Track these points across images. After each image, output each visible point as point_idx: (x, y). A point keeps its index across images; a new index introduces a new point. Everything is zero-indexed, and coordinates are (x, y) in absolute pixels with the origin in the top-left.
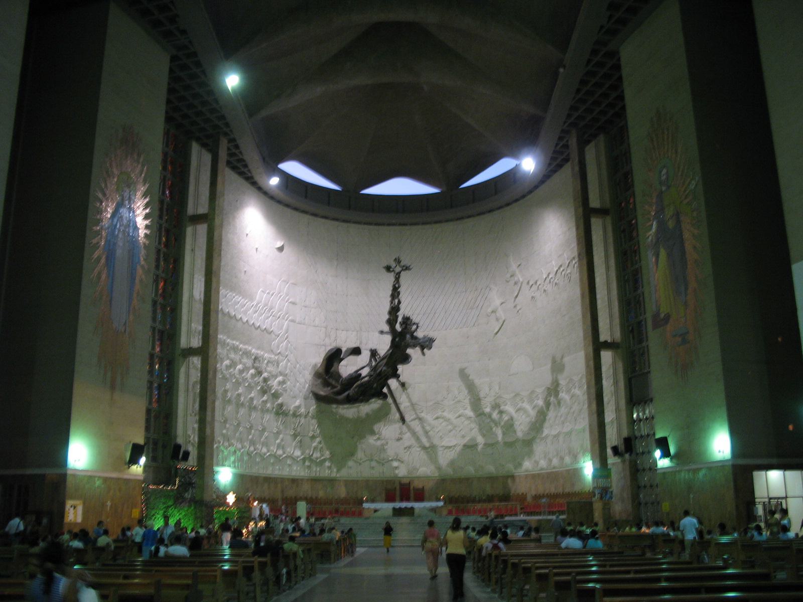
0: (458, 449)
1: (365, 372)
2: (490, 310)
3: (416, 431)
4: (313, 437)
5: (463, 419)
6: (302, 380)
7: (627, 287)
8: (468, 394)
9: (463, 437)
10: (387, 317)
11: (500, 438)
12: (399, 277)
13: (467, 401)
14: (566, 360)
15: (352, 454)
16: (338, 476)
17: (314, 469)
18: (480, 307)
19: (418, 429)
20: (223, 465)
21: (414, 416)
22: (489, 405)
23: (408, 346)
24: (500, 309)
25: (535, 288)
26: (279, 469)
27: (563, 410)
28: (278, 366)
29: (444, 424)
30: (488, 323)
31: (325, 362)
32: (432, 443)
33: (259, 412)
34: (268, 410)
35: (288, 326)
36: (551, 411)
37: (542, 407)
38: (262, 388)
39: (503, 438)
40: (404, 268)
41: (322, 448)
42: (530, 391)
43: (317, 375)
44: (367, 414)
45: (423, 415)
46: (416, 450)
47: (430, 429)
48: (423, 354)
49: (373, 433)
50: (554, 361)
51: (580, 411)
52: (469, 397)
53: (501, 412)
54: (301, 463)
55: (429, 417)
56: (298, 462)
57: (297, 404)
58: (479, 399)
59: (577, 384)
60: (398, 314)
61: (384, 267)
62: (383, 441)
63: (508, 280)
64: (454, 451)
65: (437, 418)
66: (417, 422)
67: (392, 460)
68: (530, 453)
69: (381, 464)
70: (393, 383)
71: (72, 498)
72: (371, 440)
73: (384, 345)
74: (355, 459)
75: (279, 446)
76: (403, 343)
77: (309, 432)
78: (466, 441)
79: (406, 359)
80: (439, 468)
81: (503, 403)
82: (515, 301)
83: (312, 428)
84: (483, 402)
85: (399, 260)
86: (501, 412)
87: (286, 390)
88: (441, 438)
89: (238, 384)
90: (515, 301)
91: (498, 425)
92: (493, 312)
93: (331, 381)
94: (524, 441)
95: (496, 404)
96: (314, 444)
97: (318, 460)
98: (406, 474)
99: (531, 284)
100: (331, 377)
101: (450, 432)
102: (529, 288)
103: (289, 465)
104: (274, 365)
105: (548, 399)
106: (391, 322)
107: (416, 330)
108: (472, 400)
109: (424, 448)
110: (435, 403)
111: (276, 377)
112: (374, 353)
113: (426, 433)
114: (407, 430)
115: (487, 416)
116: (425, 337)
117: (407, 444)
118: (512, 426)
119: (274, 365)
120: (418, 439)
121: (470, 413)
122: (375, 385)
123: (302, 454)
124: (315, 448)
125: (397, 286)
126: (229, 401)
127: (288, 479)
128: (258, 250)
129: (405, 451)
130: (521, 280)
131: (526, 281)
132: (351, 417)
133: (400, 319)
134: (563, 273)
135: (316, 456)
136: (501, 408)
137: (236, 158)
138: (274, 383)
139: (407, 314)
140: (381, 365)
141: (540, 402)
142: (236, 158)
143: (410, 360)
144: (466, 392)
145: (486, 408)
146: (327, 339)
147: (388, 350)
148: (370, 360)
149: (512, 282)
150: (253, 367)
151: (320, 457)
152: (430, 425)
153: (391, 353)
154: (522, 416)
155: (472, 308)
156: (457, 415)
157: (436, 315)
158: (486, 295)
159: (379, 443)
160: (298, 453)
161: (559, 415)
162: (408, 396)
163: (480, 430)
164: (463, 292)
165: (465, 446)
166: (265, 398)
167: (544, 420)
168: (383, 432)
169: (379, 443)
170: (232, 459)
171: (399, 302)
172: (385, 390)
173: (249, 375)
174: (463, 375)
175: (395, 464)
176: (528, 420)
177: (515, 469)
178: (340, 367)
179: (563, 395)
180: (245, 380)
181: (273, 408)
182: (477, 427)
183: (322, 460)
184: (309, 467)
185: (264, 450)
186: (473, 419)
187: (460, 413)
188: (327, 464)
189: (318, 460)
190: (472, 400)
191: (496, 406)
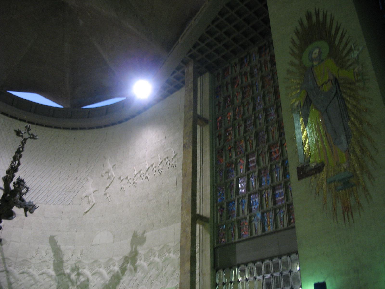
2: (84, 195)
5: (45, 276)
7: (218, 175)
8: (54, 256)
10: (5, 174)
12: (25, 142)
13: (52, 262)
14: (147, 234)
18: (76, 191)
22: (70, 267)
23: (15, 204)
24: (92, 195)
25: (125, 181)
27: (139, 274)
29: (28, 278)
30: (80, 204)
36: (127, 276)
37: (118, 272)
40: (31, 136)
42: (108, 259)
45: (11, 269)
50: (135, 235)
51: (174, 272)
52: (54, 259)
53: (79, 274)
55: (15, 271)
58: (62, 262)
59: (157, 254)
60: (15, 174)
61: (15, 131)
63: (103, 175)
65: (23, 273)
76: (13, 199)
81: (82, 266)
84: (65, 264)
85: (29, 128)
91: (75, 284)
92: (86, 196)
95: (76, 267)
99: (122, 178)
102: (120, 181)
105: (124, 266)
106: (7, 180)
108: (56, 262)
110: (24, 260)
115: (67, 276)
121: (52, 272)
125: (21, 149)
130: (114, 175)
131: (118, 177)
133: (15, 180)
134: (155, 169)
136: (80, 271)
139: (22, 177)
141: (116, 268)
143: (14, 217)
145: (67, 269)
149: (106, 177)
152: (15, 278)
154: (97, 279)
155: (70, 192)
157: (41, 192)
158: (82, 184)
161: (135, 278)
164: (65, 179)
167: (118, 283)
171: (19, 164)
174: (52, 240)
176: (102, 282)
179: (141, 262)
182: (56, 284)
186: (53, 277)
187: (44, 270)
190: (56, 262)
191: (76, 269)
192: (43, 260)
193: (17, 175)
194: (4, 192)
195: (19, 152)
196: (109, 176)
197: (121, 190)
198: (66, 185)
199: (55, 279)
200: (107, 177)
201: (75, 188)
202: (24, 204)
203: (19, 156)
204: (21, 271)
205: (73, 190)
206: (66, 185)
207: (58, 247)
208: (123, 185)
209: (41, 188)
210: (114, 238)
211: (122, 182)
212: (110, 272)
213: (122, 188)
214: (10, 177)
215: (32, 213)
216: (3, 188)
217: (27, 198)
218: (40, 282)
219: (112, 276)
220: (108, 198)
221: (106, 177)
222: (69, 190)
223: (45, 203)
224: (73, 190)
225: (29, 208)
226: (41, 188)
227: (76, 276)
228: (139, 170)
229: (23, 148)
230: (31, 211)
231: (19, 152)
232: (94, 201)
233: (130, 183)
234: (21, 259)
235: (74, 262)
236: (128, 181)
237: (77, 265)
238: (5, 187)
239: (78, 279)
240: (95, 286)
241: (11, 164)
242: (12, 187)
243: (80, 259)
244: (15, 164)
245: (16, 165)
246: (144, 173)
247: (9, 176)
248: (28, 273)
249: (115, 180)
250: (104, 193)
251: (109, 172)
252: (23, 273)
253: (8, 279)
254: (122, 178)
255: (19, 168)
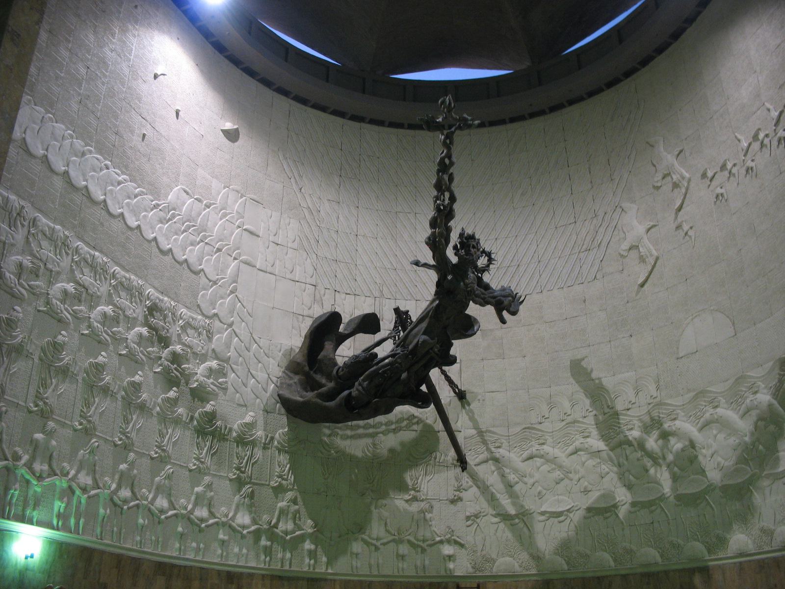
0: (577, 516)
2: (625, 246)
3: (489, 483)
4: (279, 490)
5: (583, 456)
6: (262, 376)
9: (586, 491)
10: (428, 232)
11: (667, 487)
12: (451, 143)
13: (590, 420)
15: (360, 528)
16: (330, 571)
17: (280, 555)
18: (604, 244)
19: (492, 479)
20: (22, 519)
21: (485, 455)
22: (637, 423)
24: (646, 240)
26: (198, 549)
28: (210, 339)
29: (546, 468)
31: (308, 341)
32: (522, 506)
33: (155, 420)
34: (177, 421)
35: (238, 270)
37: (770, 405)
38: (166, 371)
39: (674, 489)
41: (298, 511)
43: (293, 368)
44: (392, 451)
46: (490, 521)
47: (516, 479)
49: (402, 487)
53: (665, 436)
54: (250, 540)
55: (513, 457)
56: (243, 537)
57: (248, 419)
62: (423, 505)
64: (568, 521)
65: (530, 458)
66: (491, 466)
67: (441, 542)
68: (746, 515)
69: (419, 550)
72: (399, 501)
74: (366, 537)
75: (199, 501)
76: (462, 284)
77: (271, 478)
78: (590, 501)
79: (467, 327)
80: (537, 558)
82: (676, 218)
83: (278, 469)
84: (623, 419)
86: (665, 436)
87: (226, 389)
88: (540, 495)
89: (95, 342)
90: (676, 218)
93: (318, 377)
94: (725, 489)
95: (652, 419)
96: (282, 504)
97: (288, 537)
98: (471, 570)
100: (320, 371)
101: (557, 483)
103: (223, 542)
104: (199, 334)
106: (437, 244)
107: (486, 269)
109: (505, 517)
111: (203, 358)
113: (509, 486)
114: (471, 483)
115: (635, 444)
116: (503, 289)
117: (471, 510)
118: (693, 460)
119: (199, 334)
120: (492, 500)
122: (404, 375)
123: (254, 521)
124: (282, 512)
125: (447, 161)
126: (65, 372)
127: (219, 572)
128: (180, 113)
129: (469, 522)
132: (359, 454)
133: (454, 238)
135: (284, 528)
136: (666, 426)
138: (199, 371)
140: (416, 335)
142: (324, 389)
143: (476, 328)
144: (588, 402)
146: (316, 305)
147: (433, 301)
149: (667, 187)
150: (147, 324)
151: (293, 532)
152: (516, 471)
153: (437, 305)
154: (715, 436)
156: (571, 448)
157: (522, 269)
159: (415, 507)
160: (243, 519)
162: (472, 419)
163: (621, 477)
165: (589, 510)
166: (172, 394)
168: (424, 487)
169: (415, 507)
170: (59, 505)
171: (453, 199)
173: (132, 335)
174: (578, 370)
175: (447, 550)
176: (733, 441)
177: (710, 552)
180: (118, 340)
181: (192, 418)
183: (297, 536)
184: (268, 551)
185: (162, 502)
186: (604, 455)
187: (577, 444)
188: (308, 545)
189: (288, 537)
191: (653, 424)
192: (569, 419)
193: (457, 227)
194: (437, 274)
195: (444, 167)
196: (674, 181)
197: (718, 202)
198: (574, 237)
199: (611, 460)
200: (670, 185)
201: (599, 238)
202: (491, 295)
203: (446, 177)
204: (526, 455)
205: (596, 243)
206: (574, 237)
207: (597, 381)
208: (719, 188)
209: (519, 261)
210: (733, 324)
211: (713, 183)
212: (748, 411)
213: (717, 197)
214: (441, 234)
215: (514, 313)
216: (432, 262)
217: (494, 279)
218: (576, 472)
219: (758, 420)
220: (689, 233)
221: (667, 187)
222: (584, 247)
223: (539, 290)
224: (596, 243)
225: (506, 302)
226: (519, 261)
227: (660, 442)
228: (753, 133)
229: (449, 156)
230: (512, 309)
231: (444, 167)
232: (655, 253)
233: (737, 175)
234: (518, 429)
235: (645, 410)
236: (730, 172)
237: (655, 414)
238: (437, 262)
239: (665, 446)
240: (715, 455)
241: (435, 202)
242: (454, 260)
243: (658, 399)
244: (444, 200)
245: (447, 202)
246: (772, 134)
247: (439, 233)
248: (542, 457)
249: (692, 185)
250: (674, 226)
251: (671, 173)
252: (530, 458)
253: (503, 476)
254: (710, 174)
255: (456, 206)
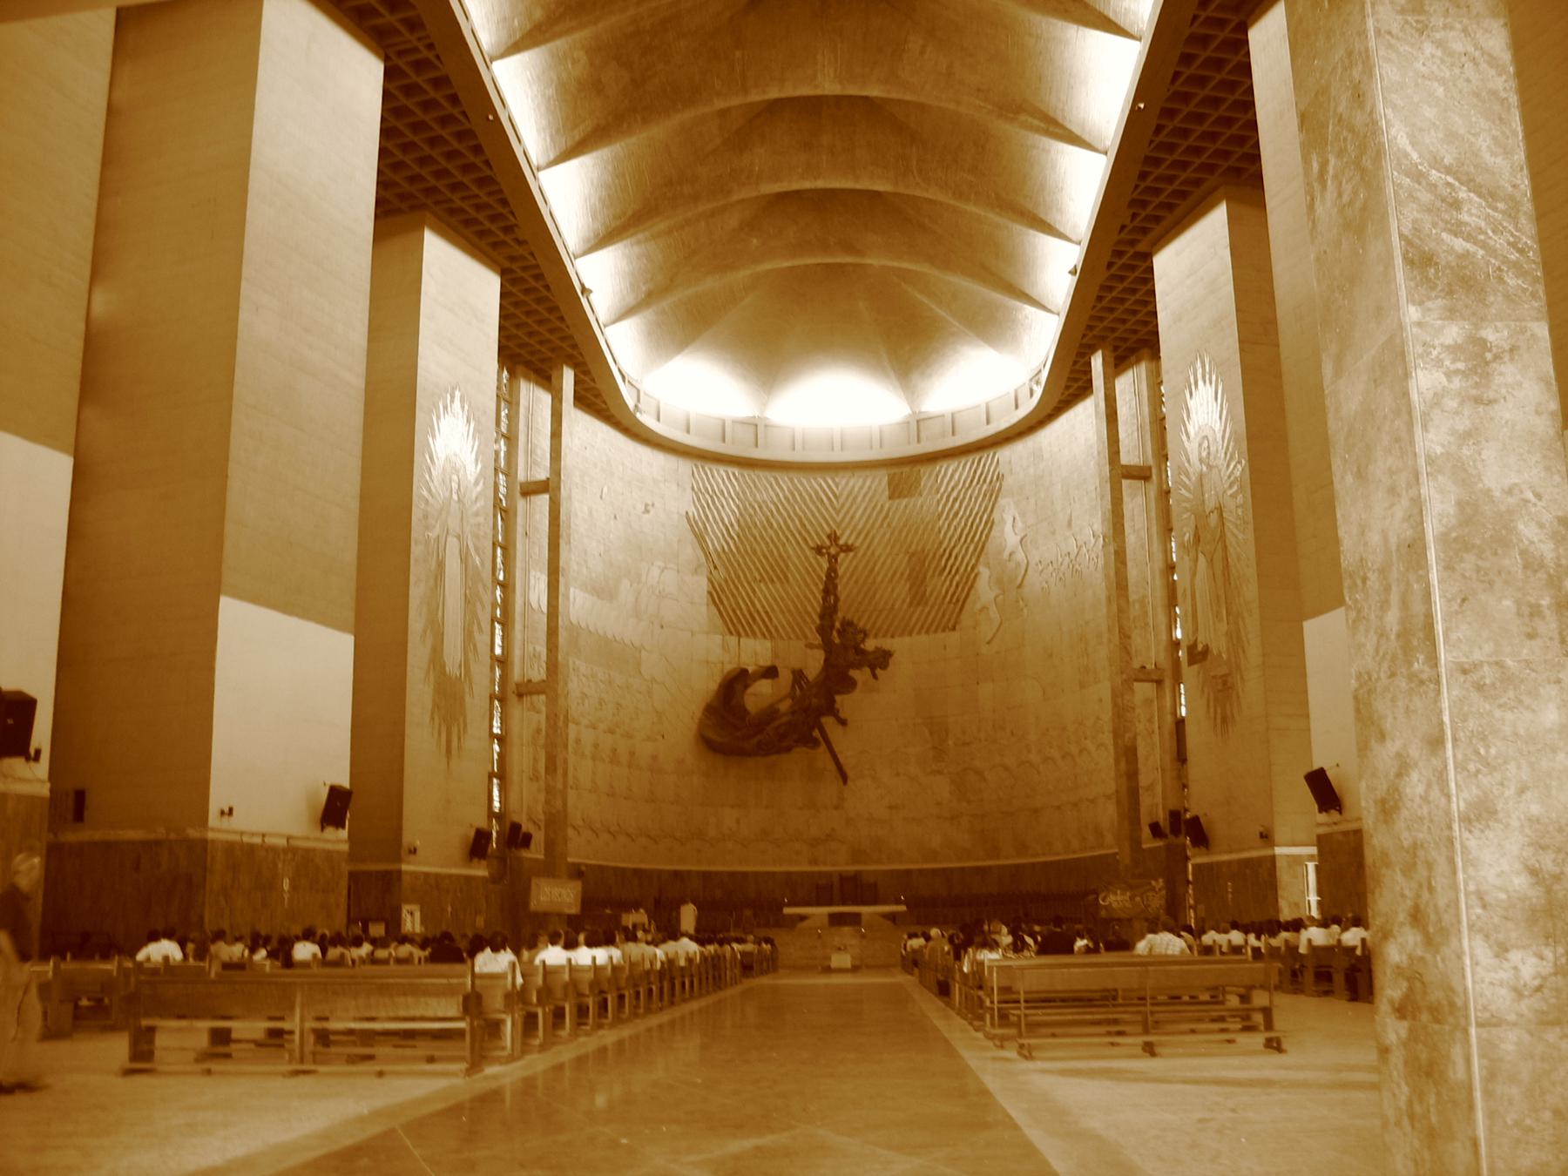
1: (784, 706)
43: (710, 710)
48: (875, 676)
70: (828, 722)
71: (409, 902)
73: (814, 663)
79: (850, 685)
106: (824, 630)
112: (798, 675)
137: (475, 176)
142: (475, 176)
148: (793, 687)
172: (816, 733)
178: (746, 697)
